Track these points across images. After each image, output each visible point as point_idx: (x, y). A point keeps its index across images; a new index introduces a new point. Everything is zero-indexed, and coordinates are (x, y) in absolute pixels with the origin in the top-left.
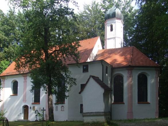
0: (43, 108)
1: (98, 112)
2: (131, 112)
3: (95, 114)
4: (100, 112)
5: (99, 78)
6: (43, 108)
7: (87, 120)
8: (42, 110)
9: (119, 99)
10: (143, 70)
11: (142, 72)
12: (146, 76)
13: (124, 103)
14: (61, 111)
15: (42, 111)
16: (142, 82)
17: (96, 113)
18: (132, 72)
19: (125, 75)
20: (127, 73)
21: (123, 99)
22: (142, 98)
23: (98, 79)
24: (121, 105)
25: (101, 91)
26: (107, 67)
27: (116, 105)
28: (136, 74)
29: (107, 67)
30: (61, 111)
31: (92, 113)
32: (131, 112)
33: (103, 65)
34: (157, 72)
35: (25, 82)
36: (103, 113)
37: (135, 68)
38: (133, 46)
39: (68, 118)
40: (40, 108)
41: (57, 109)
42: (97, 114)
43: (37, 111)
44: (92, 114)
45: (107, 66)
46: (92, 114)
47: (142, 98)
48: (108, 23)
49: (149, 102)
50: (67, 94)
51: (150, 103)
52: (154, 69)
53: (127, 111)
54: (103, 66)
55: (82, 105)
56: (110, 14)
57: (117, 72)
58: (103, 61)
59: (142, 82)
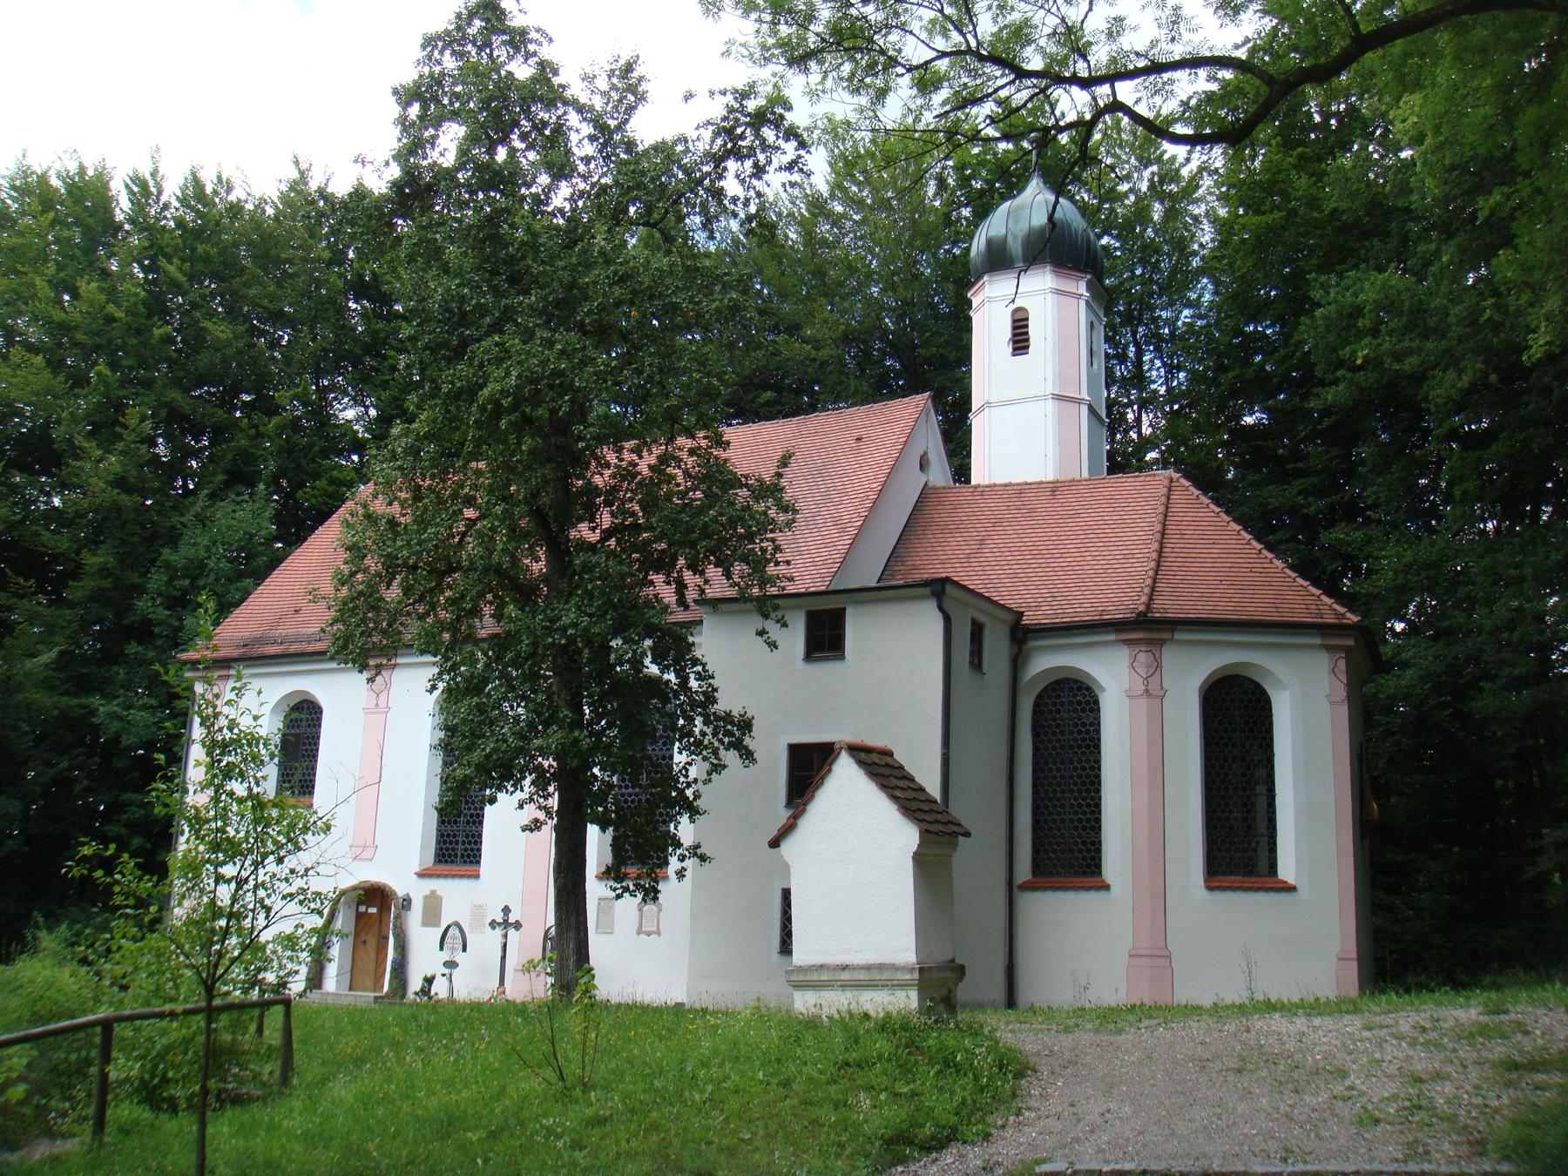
0: (506, 910)
1: (881, 967)
2: (1155, 954)
3: (862, 975)
4: (893, 967)
5: (890, 754)
6: (506, 910)
7: (804, 1002)
8: (493, 924)
9: (1067, 846)
10: (1238, 645)
11: (1236, 664)
12: (1264, 693)
13: (1106, 887)
14: (639, 932)
15: (499, 931)
16: (1236, 728)
17: (868, 968)
18: (1159, 666)
19: (1112, 674)
20: (1126, 663)
21: (1099, 851)
22: (1239, 845)
23: (887, 765)
24: (1061, 895)
25: (905, 836)
26: (977, 630)
27: (1049, 896)
28: (1188, 673)
29: (977, 630)
30: (639, 932)
31: (845, 968)
32: (1155, 954)
33: (950, 612)
34: (1342, 664)
35: (379, 709)
36: (912, 970)
37: (1177, 636)
38: (1171, 472)
39: (689, 994)
40: (478, 910)
41: (607, 928)
42: (876, 976)
43: (454, 932)
44: (845, 976)
45: (982, 618)
46: (845, 976)
47: (1239, 845)
48: (990, 300)
49: (1291, 881)
50: (685, 830)
51: (1293, 889)
52: (1317, 641)
53: (1127, 945)
54: (947, 619)
55: (786, 894)
56: (1010, 240)
57: (1046, 662)
58: (949, 589)
59: (1236, 728)
